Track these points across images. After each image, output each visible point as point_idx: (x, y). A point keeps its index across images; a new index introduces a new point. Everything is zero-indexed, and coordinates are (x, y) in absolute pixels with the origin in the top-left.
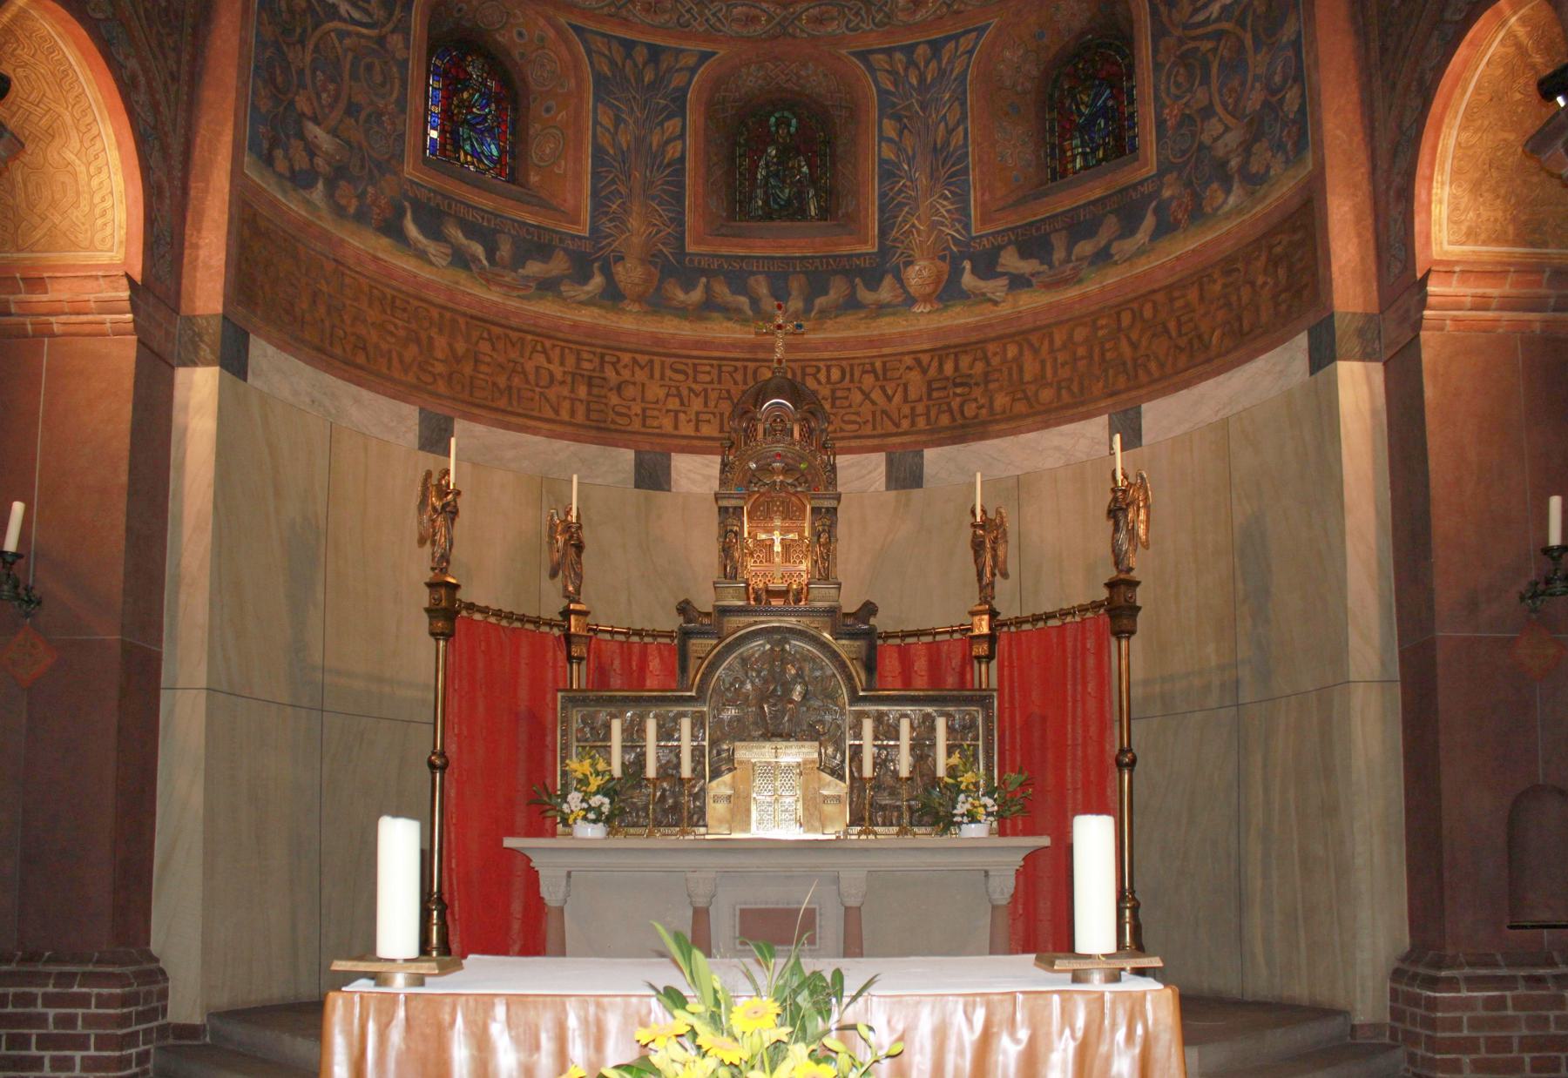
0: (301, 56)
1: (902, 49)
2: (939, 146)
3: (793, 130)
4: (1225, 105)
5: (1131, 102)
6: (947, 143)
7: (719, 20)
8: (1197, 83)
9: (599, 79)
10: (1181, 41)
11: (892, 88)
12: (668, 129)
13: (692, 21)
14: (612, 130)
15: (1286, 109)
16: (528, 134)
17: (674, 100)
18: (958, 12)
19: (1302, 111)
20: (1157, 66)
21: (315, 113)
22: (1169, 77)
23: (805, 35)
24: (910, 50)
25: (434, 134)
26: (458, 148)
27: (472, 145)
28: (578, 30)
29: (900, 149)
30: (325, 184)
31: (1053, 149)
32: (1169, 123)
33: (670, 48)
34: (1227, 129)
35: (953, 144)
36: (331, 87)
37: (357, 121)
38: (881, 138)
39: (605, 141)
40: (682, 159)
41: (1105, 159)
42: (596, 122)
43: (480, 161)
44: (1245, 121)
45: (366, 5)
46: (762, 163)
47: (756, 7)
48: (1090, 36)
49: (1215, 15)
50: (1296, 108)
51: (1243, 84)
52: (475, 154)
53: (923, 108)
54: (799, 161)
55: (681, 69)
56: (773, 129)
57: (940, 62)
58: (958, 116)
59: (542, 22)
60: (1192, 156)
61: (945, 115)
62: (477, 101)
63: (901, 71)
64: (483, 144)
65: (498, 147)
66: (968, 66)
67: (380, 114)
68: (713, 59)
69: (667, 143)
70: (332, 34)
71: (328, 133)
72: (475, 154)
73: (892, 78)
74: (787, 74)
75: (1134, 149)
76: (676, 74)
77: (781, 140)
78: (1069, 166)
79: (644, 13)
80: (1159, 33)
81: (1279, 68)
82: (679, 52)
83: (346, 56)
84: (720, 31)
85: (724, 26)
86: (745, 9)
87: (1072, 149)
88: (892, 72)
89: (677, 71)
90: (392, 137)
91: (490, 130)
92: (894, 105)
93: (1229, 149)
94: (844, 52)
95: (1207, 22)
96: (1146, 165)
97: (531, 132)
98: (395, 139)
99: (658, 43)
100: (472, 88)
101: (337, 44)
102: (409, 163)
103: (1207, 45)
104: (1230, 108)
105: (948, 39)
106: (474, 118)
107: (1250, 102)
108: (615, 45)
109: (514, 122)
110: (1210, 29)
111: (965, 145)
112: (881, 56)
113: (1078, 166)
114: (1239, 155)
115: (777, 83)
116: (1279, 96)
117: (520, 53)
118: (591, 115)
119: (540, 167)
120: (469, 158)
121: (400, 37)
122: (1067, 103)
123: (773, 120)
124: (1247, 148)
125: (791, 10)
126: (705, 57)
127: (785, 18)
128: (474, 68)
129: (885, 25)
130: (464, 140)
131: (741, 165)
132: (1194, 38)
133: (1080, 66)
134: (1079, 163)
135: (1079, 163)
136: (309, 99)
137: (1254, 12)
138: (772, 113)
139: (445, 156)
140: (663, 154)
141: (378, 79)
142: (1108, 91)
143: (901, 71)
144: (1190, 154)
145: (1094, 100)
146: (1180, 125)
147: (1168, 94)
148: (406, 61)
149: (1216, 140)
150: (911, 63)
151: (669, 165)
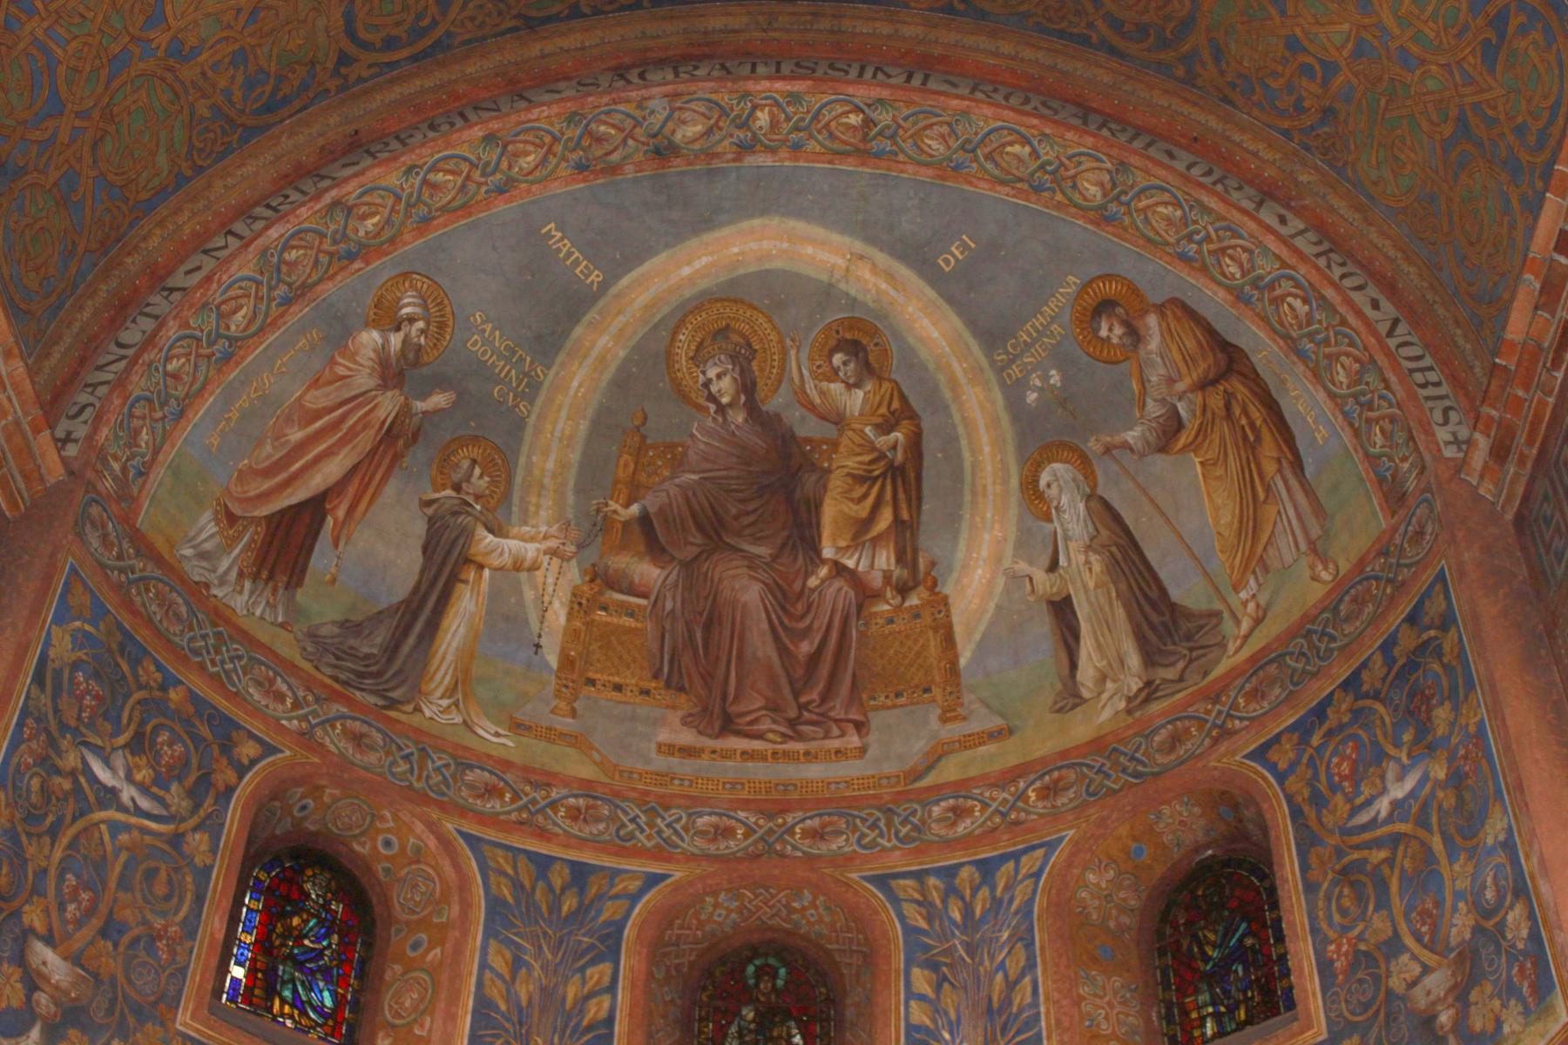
0: (46, 851)
1: (938, 872)
2: (995, 1005)
3: (780, 983)
4: (1418, 938)
5: (1280, 939)
6: (1007, 1001)
7: (676, 832)
8: (1371, 908)
9: (496, 906)
10: (1340, 853)
11: (922, 924)
12: (591, 978)
13: (637, 833)
14: (507, 978)
15: (1509, 936)
16: (381, 978)
17: (602, 939)
18: (1017, 823)
19: (1535, 936)
20: (1310, 888)
21: (50, 930)
22: (1328, 899)
23: (799, 854)
24: (950, 873)
25: (238, 972)
26: (271, 992)
27: (295, 991)
28: (472, 840)
29: (936, 1009)
30: (42, 1030)
31: (1169, 1009)
32: (1338, 965)
33: (603, 868)
34: (1427, 969)
35: (1016, 1002)
36: (85, 896)
37: (116, 946)
38: (910, 995)
39: (495, 992)
40: (610, 1020)
41: (1250, 1021)
42: (484, 966)
43: (304, 1013)
44: (1452, 956)
45: (161, 793)
46: (733, 1029)
47: (732, 818)
48: (1210, 852)
49: (1383, 814)
50: (1524, 933)
51: (1438, 904)
52: (297, 1003)
53: (971, 954)
54: (789, 1028)
55: (617, 896)
56: (751, 982)
57: (993, 888)
58: (1022, 963)
59: (419, 827)
60: (1378, 1011)
61: (1003, 962)
62: (311, 929)
63: (938, 902)
64: (312, 990)
65: (334, 994)
66: (1034, 891)
67: (154, 937)
68: (664, 884)
69: (588, 997)
70: (103, 827)
71: (65, 959)
72: (297, 1003)
73: (924, 911)
74: (773, 906)
75: (1291, 1005)
76: (610, 903)
77: (762, 999)
78: (1196, 1033)
79: (568, 821)
80: (1307, 842)
81: (1489, 879)
82: (615, 873)
83: (117, 856)
84: (677, 847)
85: (682, 840)
86: (714, 819)
87: (1199, 1008)
88: (925, 903)
89: (611, 898)
90: (167, 972)
91: (326, 973)
92: (927, 948)
93: (1432, 997)
94: (854, 876)
95: (1373, 825)
96: (1310, 1027)
97: (388, 976)
98: (171, 975)
99: (585, 860)
100: (308, 912)
101: (107, 837)
102: (185, 1009)
103: (1380, 855)
104: (1426, 939)
105: (1004, 858)
106: (302, 954)
107: (1454, 930)
108: (522, 862)
109: (363, 962)
110: (1379, 832)
111: (1035, 1004)
112: (908, 882)
113: (1209, 1032)
114: (1448, 1007)
115: (759, 918)
116: (1497, 919)
117: (383, 869)
118: (477, 954)
119: (393, 1026)
120: (287, 1009)
121: (206, 837)
122: (1185, 944)
123: (751, 969)
124: (1460, 994)
125: (780, 821)
126: (653, 880)
127: (771, 831)
128: (314, 884)
129: (914, 840)
130: (284, 983)
131: (700, 1032)
132: (1357, 847)
133: (1200, 893)
134: (1210, 1028)
135: (1210, 1028)
136: (46, 911)
137: (1440, 808)
138: (750, 960)
139: (250, 1004)
140: (582, 1012)
141: (160, 889)
142: (1244, 926)
143: (938, 902)
144: (1375, 1008)
145: (1225, 936)
146: (1353, 966)
147: (1330, 925)
148: (209, 869)
149: (1412, 984)
150: (951, 891)
151: (589, 1028)
